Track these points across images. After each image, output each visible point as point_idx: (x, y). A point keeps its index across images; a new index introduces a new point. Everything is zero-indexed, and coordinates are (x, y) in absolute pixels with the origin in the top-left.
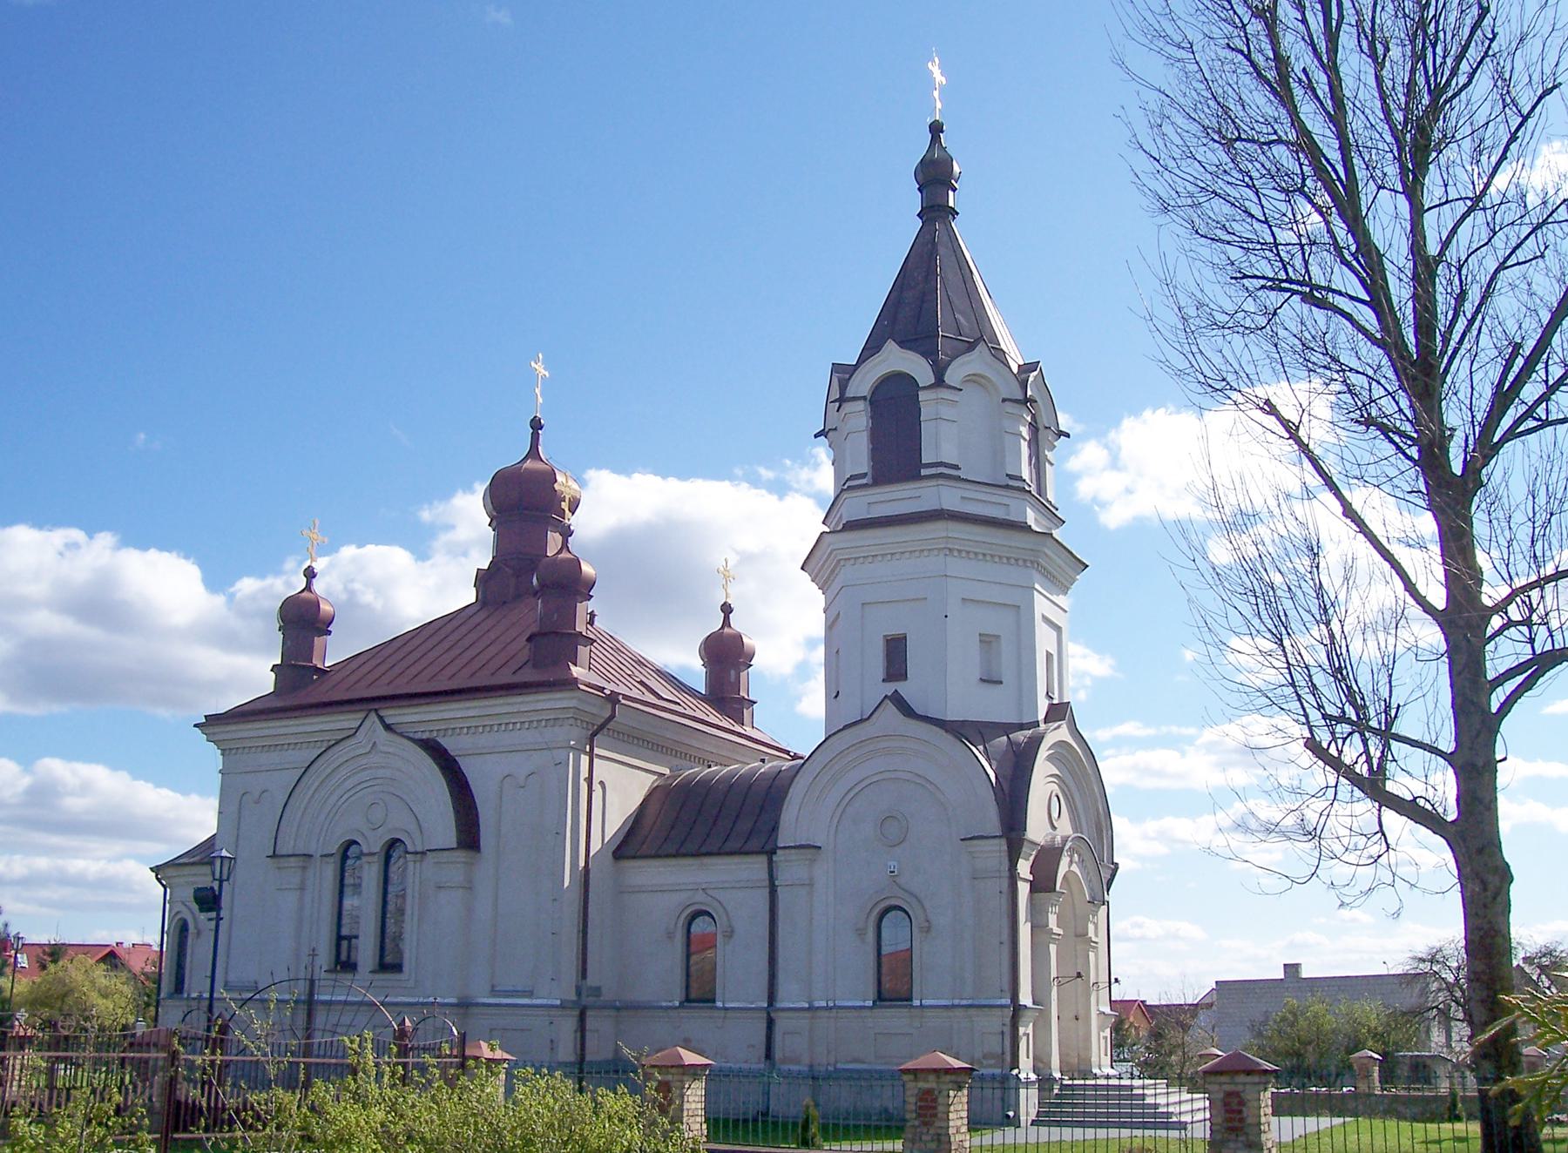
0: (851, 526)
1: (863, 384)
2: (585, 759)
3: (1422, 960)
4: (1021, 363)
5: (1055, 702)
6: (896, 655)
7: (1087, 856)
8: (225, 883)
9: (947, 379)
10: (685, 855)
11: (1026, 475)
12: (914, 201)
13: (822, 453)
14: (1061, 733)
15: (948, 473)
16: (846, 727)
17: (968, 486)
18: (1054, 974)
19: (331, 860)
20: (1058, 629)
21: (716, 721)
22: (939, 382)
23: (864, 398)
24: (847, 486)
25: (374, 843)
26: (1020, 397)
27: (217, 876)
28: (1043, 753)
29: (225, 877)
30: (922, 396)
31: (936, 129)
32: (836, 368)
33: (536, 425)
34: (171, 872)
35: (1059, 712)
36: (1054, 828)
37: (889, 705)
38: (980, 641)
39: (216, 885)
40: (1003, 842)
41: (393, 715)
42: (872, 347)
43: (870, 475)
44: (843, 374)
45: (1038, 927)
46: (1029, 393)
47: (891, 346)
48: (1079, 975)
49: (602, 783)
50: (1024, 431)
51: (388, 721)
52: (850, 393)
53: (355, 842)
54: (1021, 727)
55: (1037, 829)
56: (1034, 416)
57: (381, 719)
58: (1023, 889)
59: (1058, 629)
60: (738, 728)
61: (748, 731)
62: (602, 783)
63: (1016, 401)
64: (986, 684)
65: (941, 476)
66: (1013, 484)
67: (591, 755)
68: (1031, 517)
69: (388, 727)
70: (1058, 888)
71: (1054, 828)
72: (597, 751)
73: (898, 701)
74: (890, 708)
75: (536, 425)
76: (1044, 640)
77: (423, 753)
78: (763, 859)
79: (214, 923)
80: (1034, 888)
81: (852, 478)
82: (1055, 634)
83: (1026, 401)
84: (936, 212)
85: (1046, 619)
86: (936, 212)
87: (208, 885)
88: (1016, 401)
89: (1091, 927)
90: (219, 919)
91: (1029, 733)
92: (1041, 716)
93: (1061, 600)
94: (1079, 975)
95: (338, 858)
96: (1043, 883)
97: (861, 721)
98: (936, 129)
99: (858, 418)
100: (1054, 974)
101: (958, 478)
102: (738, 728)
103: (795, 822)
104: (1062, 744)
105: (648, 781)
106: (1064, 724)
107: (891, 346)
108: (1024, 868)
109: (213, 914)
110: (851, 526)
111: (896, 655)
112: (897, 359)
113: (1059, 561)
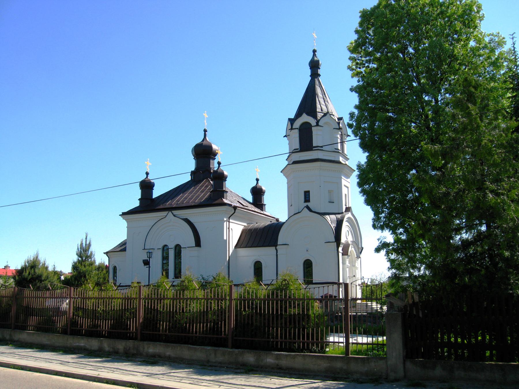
0: (295, 162)
1: (298, 124)
2: (228, 223)
3: (94, 256)
4: (338, 117)
5: (347, 206)
6: (307, 194)
7: (355, 245)
8: (150, 259)
9: (320, 124)
10: (247, 247)
11: (339, 148)
12: (309, 72)
13: (286, 140)
14: (349, 215)
15: (319, 148)
16: (295, 214)
17: (325, 152)
18: (348, 276)
19: (160, 250)
20: (348, 187)
21: (253, 209)
22: (317, 125)
23: (298, 128)
24: (293, 152)
25: (172, 245)
26: (338, 127)
27: (149, 257)
28: (345, 220)
29: (150, 257)
30: (313, 128)
31: (314, 51)
32: (290, 120)
33: (205, 131)
34: (110, 254)
35: (348, 209)
36: (347, 239)
37: (305, 209)
38: (329, 192)
39: (148, 259)
40: (336, 243)
41: (176, 212)
42: (299, 114)
43: (299, 149)
44: (292, 121)
45: (344, 263)
46: (341, 125)
47: (304, 115)
48: (354, 276)
49: (231, 229)
50: (339, 136)
51: (174, 214)
52: (294, 127)
53: (166, 245)
54: (339, 214)
55: (343, 240)
56: (341, 132)
57: (172, 213)
58: (340, 255)
59: (348, 187)
60: (262, 212)
61: (265, 213)
62: (231, 229)
63: (337, 129)
64: (330, 203)
65: (318, 150)
66: (336, 151)
67: (229, 222)
68: (341, 159)
69: (174, 216)
70: (349, 254)
71: (347, 239)
72: (231, 221)
73: (308, 208)
74: (306, 209)
75: (205, 131)
76: (344, 191)
77: (184, 222)
78: (274, 248)
79: (148, 268)
80: (343, 254)
81: (295, 150)
82: (347, 189)
83: (340, 129)
84: (315, 75)
85: (345, 186)
86: (315, 75)
87: (147, 259)
88: (337, 129)
89: (356, 264)
90: (149, 267)
91: (340, 215)
92: (344, 210)
93: (348, 180)
94: (354, 276)
95: (162, 249)
96: (345, 253)
97: (299, 213)
98: (314, 51)
99: (296, 134)
100: (348, 276)
101: (322, 150)
102: (262, 212)
103: (282, 238)
104: (349, 218)
105: (242, 228)
106: (350, 213)
107: (304, 115)
108: (340, 249)
109: (148, 266)
110: (295, 162)
111: (307, 194)
112: (305, 118)
113: (347, 171)
